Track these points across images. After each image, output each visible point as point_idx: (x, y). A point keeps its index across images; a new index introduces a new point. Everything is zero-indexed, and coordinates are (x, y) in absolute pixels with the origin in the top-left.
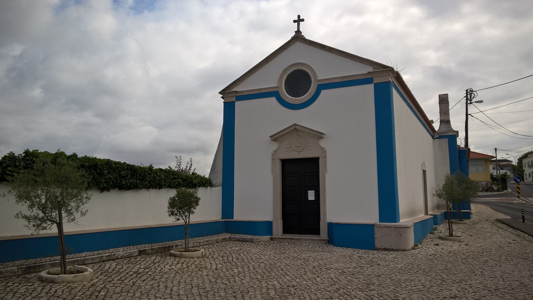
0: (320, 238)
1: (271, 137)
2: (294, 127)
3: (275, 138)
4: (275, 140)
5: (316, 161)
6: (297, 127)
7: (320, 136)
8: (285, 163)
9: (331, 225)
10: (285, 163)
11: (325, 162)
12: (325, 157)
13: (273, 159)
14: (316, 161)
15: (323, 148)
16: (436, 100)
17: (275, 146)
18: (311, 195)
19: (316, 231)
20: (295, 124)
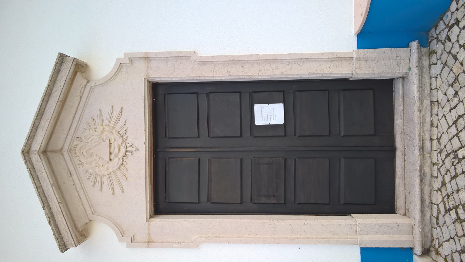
0: (415, 71)
1: (64, 247)
2: (35, 158)
3: (72, 230)
4: (82, 235)
5: (162, 96)
6: (37, 145)
7: (71, 72)
8: (163, 203)
9: (369, 36)
10: (163, 203)
11: (166, 58)
12: (147, 58)
13: (149, 243)
14: (162, 96)
15: (120, 67)
16: (120, 108)
17: (103, 233)
18: (270, 114)
19: (380, 92)
20: (26, 152)
